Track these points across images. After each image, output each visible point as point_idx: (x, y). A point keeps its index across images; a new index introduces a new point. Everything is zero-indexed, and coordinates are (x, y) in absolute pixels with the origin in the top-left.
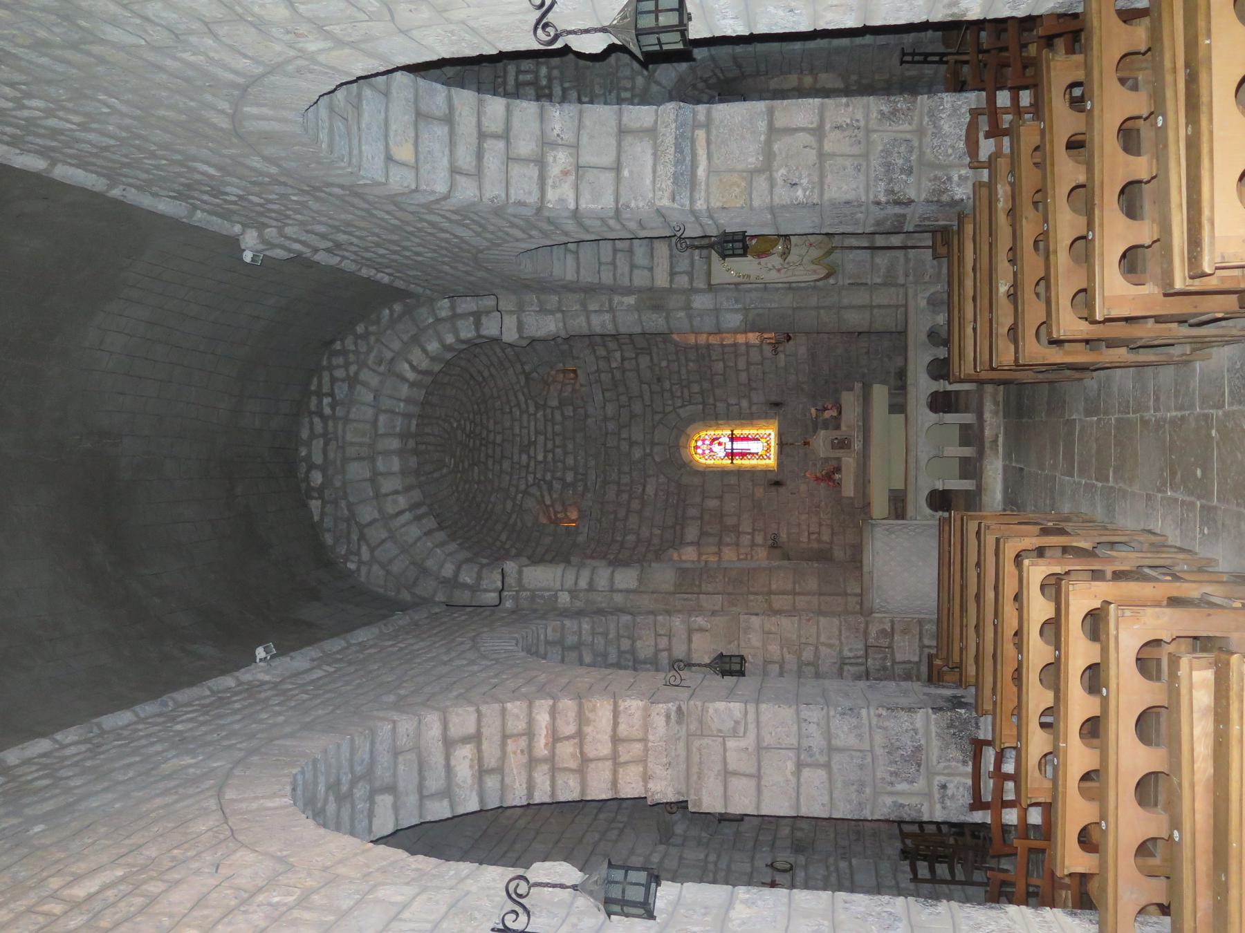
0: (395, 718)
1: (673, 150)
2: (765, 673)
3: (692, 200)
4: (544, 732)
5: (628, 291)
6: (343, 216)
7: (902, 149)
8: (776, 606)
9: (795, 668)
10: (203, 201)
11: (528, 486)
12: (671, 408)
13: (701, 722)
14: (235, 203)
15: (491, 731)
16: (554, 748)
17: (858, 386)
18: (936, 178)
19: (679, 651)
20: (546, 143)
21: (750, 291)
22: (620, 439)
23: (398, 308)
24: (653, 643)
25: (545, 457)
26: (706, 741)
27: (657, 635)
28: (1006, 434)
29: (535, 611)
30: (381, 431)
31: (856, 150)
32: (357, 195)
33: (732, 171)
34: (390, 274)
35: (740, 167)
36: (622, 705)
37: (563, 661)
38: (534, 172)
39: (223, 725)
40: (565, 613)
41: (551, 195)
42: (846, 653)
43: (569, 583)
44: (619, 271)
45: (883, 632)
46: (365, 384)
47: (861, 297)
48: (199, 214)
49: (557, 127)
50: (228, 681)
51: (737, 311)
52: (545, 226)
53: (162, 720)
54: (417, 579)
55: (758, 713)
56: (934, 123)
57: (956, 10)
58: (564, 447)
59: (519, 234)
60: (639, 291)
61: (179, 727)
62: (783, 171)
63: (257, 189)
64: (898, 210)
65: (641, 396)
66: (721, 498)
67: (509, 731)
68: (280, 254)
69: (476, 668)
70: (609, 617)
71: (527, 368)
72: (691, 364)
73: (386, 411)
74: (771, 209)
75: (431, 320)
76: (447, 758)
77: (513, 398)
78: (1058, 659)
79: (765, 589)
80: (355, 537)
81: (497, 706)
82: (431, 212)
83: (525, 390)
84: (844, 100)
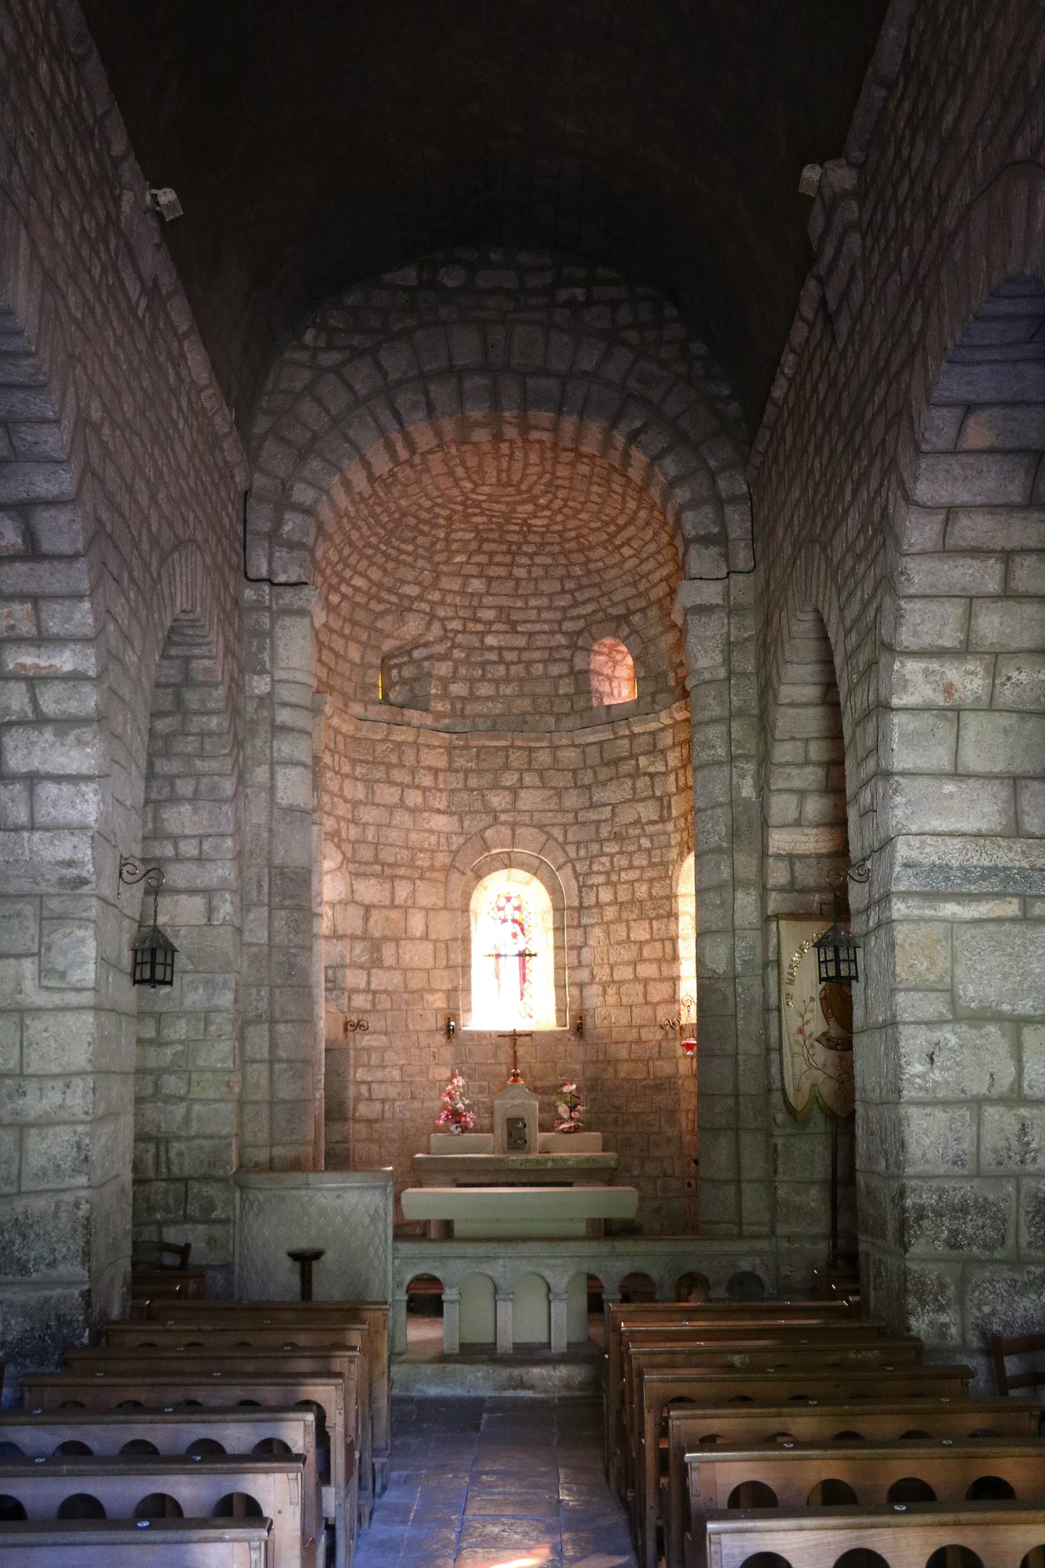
0: (65, 423)
1: (987, 863)
2: (141, 1015)
4: (43, 663)
5: (763, 787)
6: (877, 329)
7: (990, 1232)
9: (152, 1063)
10: (901, 100)
11: (443, 620)
12: (572, 854)
14: (898, 154)
15: (47, 577)
17: (611, 1157)
18: (943, 1286)
19: (177, 875)
20: (996, 659)
21: (764, 984)
22: (521, 771)
23: (733, 409)
24: (187, 832)
25: (491, 649)
27: (201, 838)
28: (533, 1401)
29: (238, 638)
30: (531, 383)
31: (988, 1157)
32: (912, 352)
33: (954, 959)
35: (959, 971)
36: (88, 789)
37: (158, 685)
38: (950, 639)
39: (48, 140)
40: (236, 687)
41: (912, 668)
42: (176, 1147)
43: (285, 693)
44: (795, 771)
45: (210, 1206)
47: (753, 1164)
48: (880, 93)
49: (1023, 677)
50: (119, 146)
51: (732, 962)
52: (862, 659)
53: (54, 37)
55: (78, 1008)
56: (1031, 1284)
58: (507, 680)
59: (850, 614)
60: (764, 806)
61: (43, 68)
62: (953, 1041)
63: (919, 192)
64: (891, 1226)
65: (592, 806)
66: (426, 937)
68: (816, 224)
69: (145, 546)
70: (230, 761)
71: (636, 618)
72: (644, 888)
73: (563, 392)
74: (893, 1023)
75: (712, 463)
78: (30, 1460)
79: (278, 1015)
80: (356, 341)
81: (85, 585)
82: (885, 473)
83: (600, 616)
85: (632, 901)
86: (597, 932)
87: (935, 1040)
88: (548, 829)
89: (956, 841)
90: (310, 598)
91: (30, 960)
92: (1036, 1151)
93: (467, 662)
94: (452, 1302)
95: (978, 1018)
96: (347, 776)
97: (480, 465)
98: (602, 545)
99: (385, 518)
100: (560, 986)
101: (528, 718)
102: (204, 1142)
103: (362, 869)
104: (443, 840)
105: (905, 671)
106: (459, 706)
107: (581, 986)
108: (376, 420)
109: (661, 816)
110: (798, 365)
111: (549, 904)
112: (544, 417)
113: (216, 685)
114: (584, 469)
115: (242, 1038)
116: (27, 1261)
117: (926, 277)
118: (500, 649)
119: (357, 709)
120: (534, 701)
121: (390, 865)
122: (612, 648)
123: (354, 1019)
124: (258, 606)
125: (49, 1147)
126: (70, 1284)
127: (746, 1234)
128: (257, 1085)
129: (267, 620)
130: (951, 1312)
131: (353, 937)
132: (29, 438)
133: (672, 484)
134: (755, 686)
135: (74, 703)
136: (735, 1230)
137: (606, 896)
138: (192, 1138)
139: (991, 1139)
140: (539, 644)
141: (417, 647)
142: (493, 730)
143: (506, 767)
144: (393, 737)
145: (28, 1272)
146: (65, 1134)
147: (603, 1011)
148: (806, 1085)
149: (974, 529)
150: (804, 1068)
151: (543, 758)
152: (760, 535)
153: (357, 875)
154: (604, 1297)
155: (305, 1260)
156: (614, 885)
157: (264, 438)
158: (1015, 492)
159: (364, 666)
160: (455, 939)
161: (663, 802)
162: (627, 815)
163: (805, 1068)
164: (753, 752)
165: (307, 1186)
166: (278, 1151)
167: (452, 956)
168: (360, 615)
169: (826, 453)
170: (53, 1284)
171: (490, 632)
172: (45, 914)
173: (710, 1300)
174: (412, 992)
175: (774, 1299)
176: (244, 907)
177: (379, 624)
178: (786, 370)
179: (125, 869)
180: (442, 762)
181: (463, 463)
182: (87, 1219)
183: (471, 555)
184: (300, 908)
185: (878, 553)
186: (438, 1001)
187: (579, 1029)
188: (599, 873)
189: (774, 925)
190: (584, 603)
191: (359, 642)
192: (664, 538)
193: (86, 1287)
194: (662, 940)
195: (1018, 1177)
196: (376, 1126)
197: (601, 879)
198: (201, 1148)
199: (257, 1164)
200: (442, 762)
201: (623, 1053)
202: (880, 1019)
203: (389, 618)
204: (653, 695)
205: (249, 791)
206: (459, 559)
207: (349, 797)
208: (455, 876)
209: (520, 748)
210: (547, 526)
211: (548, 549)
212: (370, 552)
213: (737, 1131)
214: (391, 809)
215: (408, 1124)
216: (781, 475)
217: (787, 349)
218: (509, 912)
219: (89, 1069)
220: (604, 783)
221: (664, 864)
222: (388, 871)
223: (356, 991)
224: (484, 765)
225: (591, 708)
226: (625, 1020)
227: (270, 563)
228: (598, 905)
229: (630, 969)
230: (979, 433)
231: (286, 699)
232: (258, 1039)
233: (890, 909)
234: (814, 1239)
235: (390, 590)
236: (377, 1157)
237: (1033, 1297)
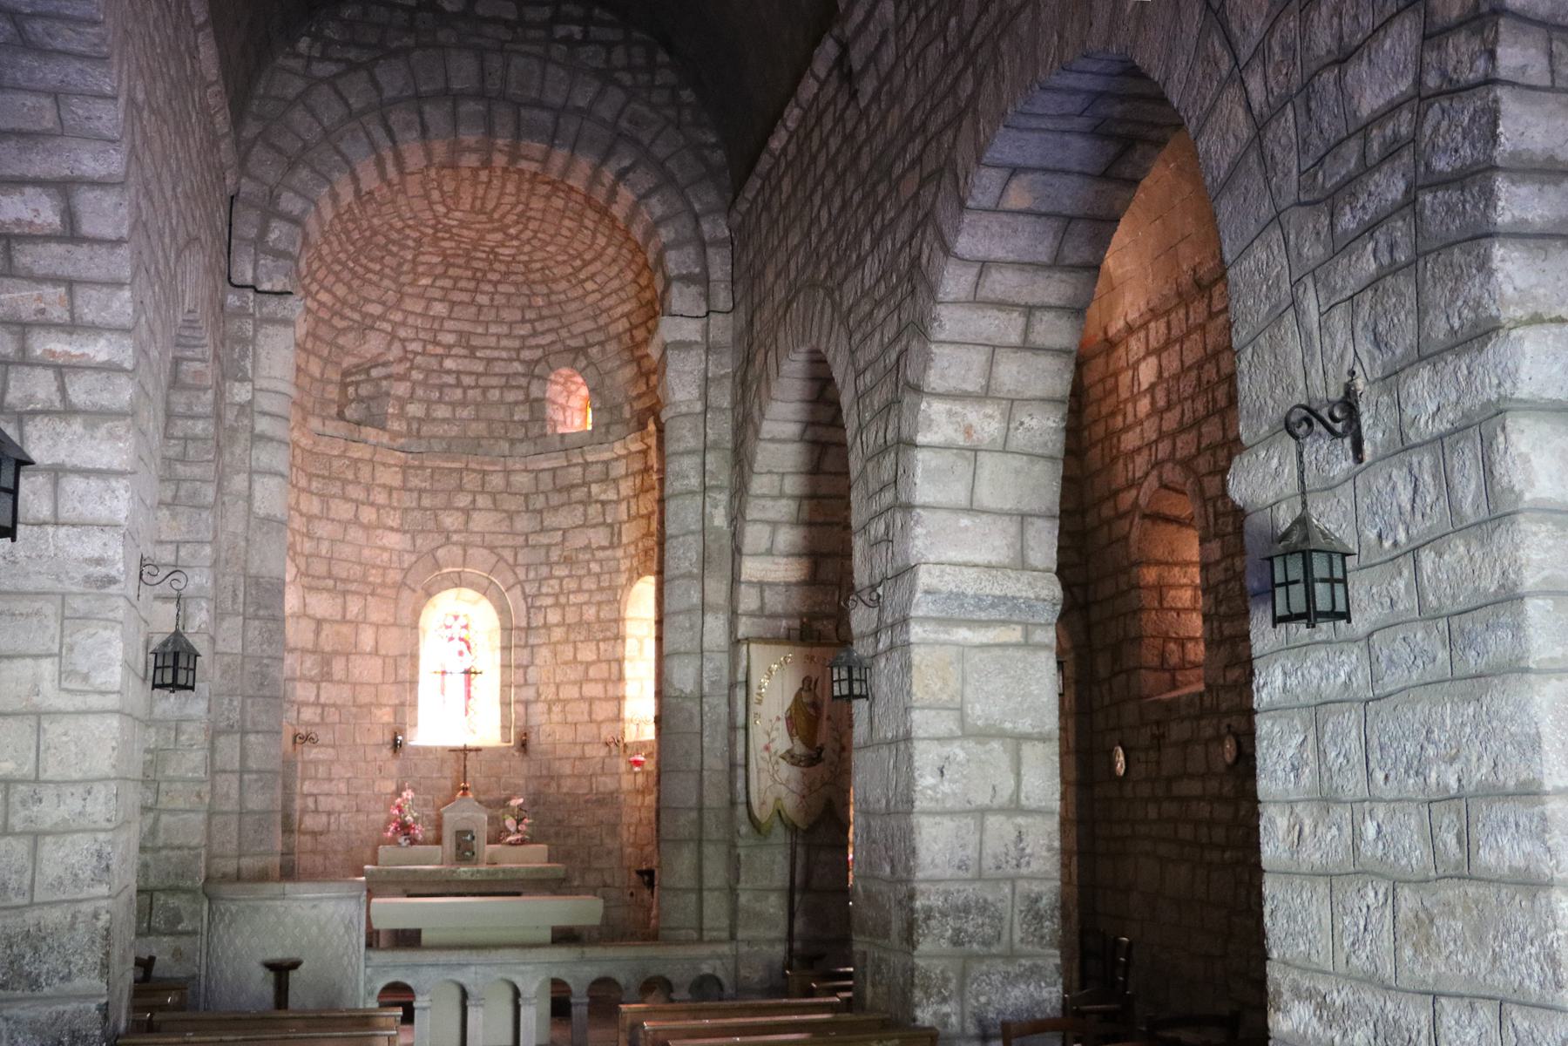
1: (998, 593)
3: (925, 619)
4: (74, 351)
5: (737, 518)
8: (222, 741)
11: (403, 341)
13: (85, 618)
15: (82, 261)
16: (46, 366)
18: (946, 980)
20: (1012, 404)
21: (731, 703)
22: (474, 493)
23: (718, 157)
25: (449, 372)
26: (53, 626)
27: (178, 545)
30: (523, 112)
31: (989, 862)
32: (959, 115)
33: (964, 680)
34: (784, 150)
35: (969, 691)
36: (119, 485)
38: (973, 384)
43: (265, 402)
44: (769, 503)
46: (601, 93)
47: (715, 872)
49: (1034, 423)
54: (280, 151)
57: (1286, 996)
58: (464, 403)
59: (863, 358)
60: (736, 536)
62: (961, 755)
64: (896, 926)
66: (375, 652)
67: (82, 293)
69: (167, 240)
71: (594, 351)
73: (556, 123)
74: (908, 738)
75: (697, 207)
76: (37, 182)
77: (547, 325)
79: (249, 725)
80: (352, 54)
81: (126, 273)
83: (558, 346)
84: (1057, 844)
85: (580, 623)
86: (544, 653)
87: (945, 754)
88: (499, 550)
89: (971, 570)
90: (295, 307)
91: (49, 660)
92: (1030, 856)
93: (424, 383)
94: (424, 1009)
95: (983, 735)
96: (303, 490)
97: (456, 191)
98: (567, 278)
99: (356, 235)
100: (505, 704)
101: (483, 442)
102: (171, 854)
103: (315, 583)
104: (395, 558)
105: (931, 411)
106: (415, 426)
107: (526, 703)
108: (368, 134)
109: (611, 543)
110: (803, 121)
111: (497, 623)
112: (536, 147)
113: (205, 389)
114: (558, 203)
115: (213, 749)
116: (39, 975)
117: (980, 46)
118: (458, 373)
119: (315, 423)
120: (489, 426)
121: (344, 581)
122: (568, 379)
123: (303, 731)
124: (241, 313)
125: (59, 858)
126: (87, 997)
127: (706, 938)
128: (227, 796)
129: (250, 328)
130: (952, 1003)
131: (304, 651)
132: (80, 112)
133: (658, 223)
134: (730, 419)
135: (106, 395)
136: (695, 936)
137: (554, 617)
138: (158, 850)
139: (993, 846)
140: (497, 370)
141: (375, 366)
142: (448, 452)
143: (460, 488)
144: (349, 454)
145: (40, 987)
146: (85, 842)
147: (547, 729)
148: (770, 800)
149: (1003, 283)
150: (773, 780)
151: (497, 481)
152: (746, 279)
153: (310, 588)
154: (573, 1000)
155: (281, 970)
156: (563, 607)
157: (254, 142)
158: (1043, 253)
159: (324, 381)
160: (404, 655)
161: (614, 529)
162: (577, 539)
163: (770, 783)
164: (726, 483)
165: (283, 896)
166: (246, 862)
167: (401, 672)
168: (323, 331)
169: (837, 203)
170: (68, 998)
171: (448, 356)
172: (67, 613)
173: (672, 1001)
174: (360, 707)
175: (733, 999)
176: (219, 616)
177: (341, 341)
178: (789, 124)
179: (146, 570)
180: (396, 481)
181: (440, 187)
182: (107, 930)
183: (436, 278)
184: (274, 619)
185: (903, 300)
186: (385, 716)
187: (523, 745)
188: (547, 595)
189: (744, 648)
190: (543, 333)
191: (320, 357)
192: (630, 276)
193: (104, 1001)
194: (609, 661)
195: (1013, 880)
196: (322, 839)
197: (550, 601)
198: (168, 859)
199: (224, 876)
200: (396, 481)
201: (567, 769)
202: (890, 735)
203: (351, 335)
204: (608, 426)
205: (226, 499)
206: (424, 281)
207: (304, 510)
208: (406, 594)
209: (474, 471)
210: (514, 256)
211: (513, 278)
212: (338, 268)
213: (700, 842)
214: (345, 524)
215: (353, 837)
216: (774, 222)
217: (793, 102)
218: (457, 631)
219: (113, 774)
220: (556, 509)
221: (612, 588)
222: (340, 586)
223: (306, 704)
224: (437, 486)
225: (545, 435)
226: (569, 737)
227: (255, 270)
228: (546, 626)
229: (576, 689)
230: (1018, 197)
231: (266, 408)
232: (229, 748)
233: (907, 632)
234: (771, 942)
235: (353, 308)
236: (321, 869)
237: (1023, 986)
